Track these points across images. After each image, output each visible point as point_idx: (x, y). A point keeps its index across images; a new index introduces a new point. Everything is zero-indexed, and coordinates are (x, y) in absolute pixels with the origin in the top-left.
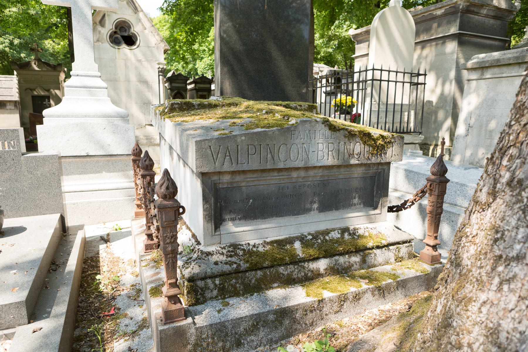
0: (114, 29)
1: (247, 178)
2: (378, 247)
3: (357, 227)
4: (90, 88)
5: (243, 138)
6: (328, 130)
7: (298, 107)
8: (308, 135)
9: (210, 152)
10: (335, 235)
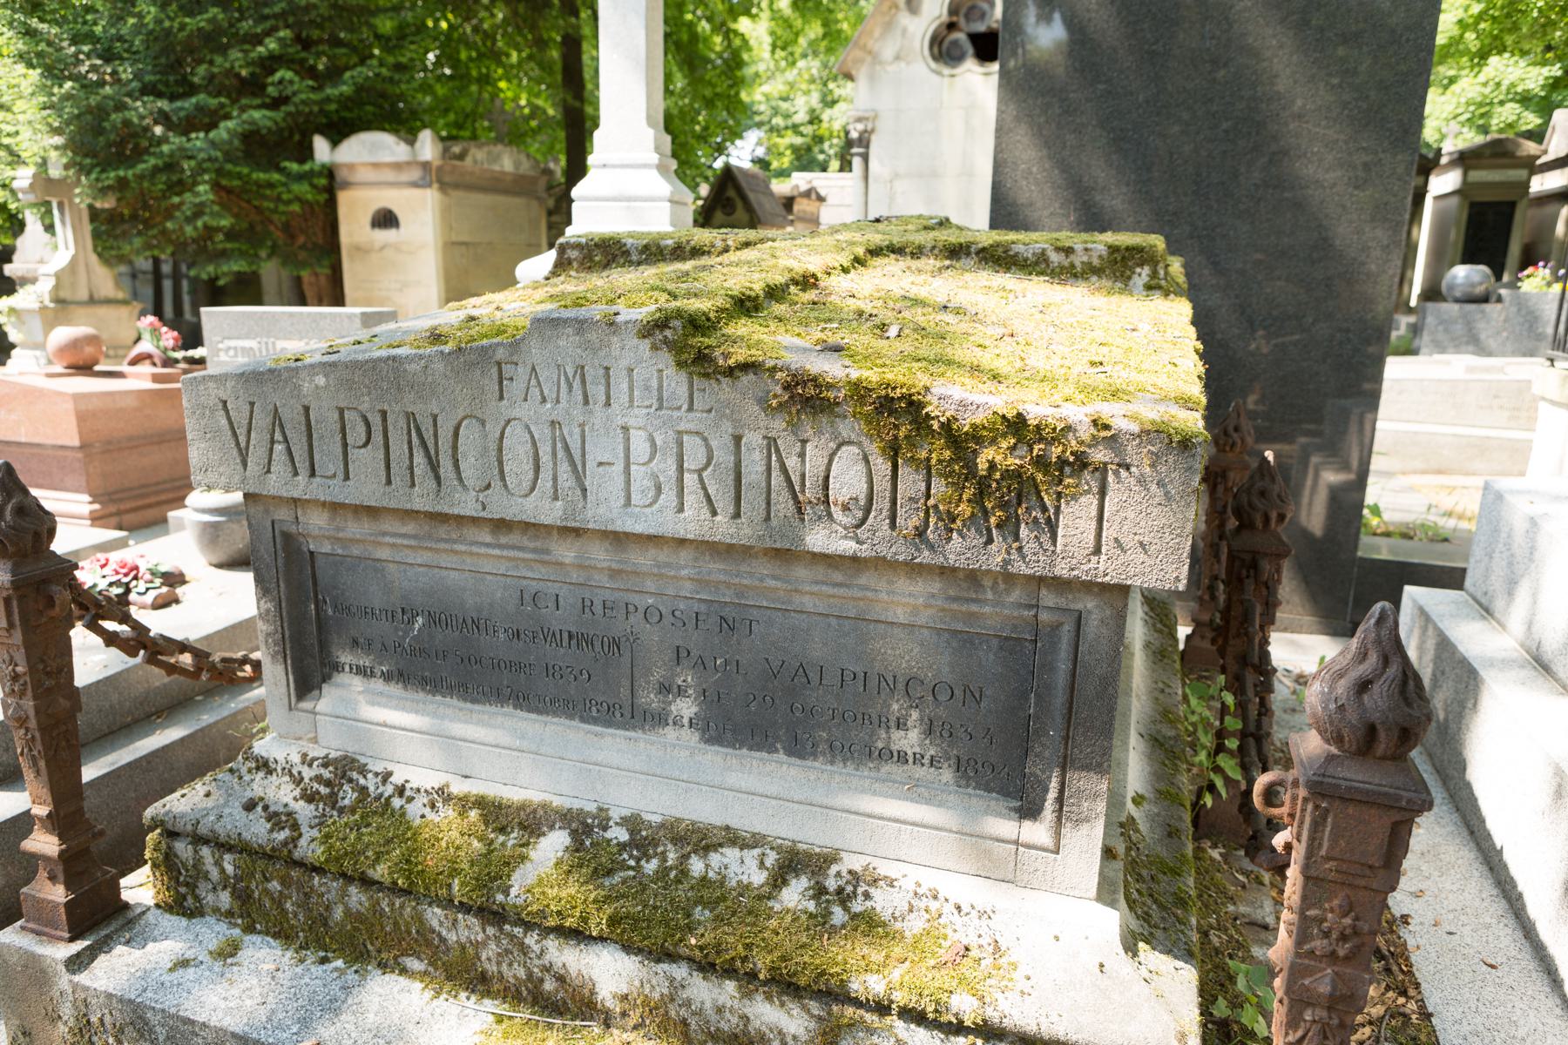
0: (945, 18)
1: (384, 534)
2: (915, 1016)
3: (885, 868)
4: (629, 199)
5: (321, 380)
6: (670, 370)
7: (1055, 258)
8: (577, 384)
9: (224, 422)
10: (746, 869)
